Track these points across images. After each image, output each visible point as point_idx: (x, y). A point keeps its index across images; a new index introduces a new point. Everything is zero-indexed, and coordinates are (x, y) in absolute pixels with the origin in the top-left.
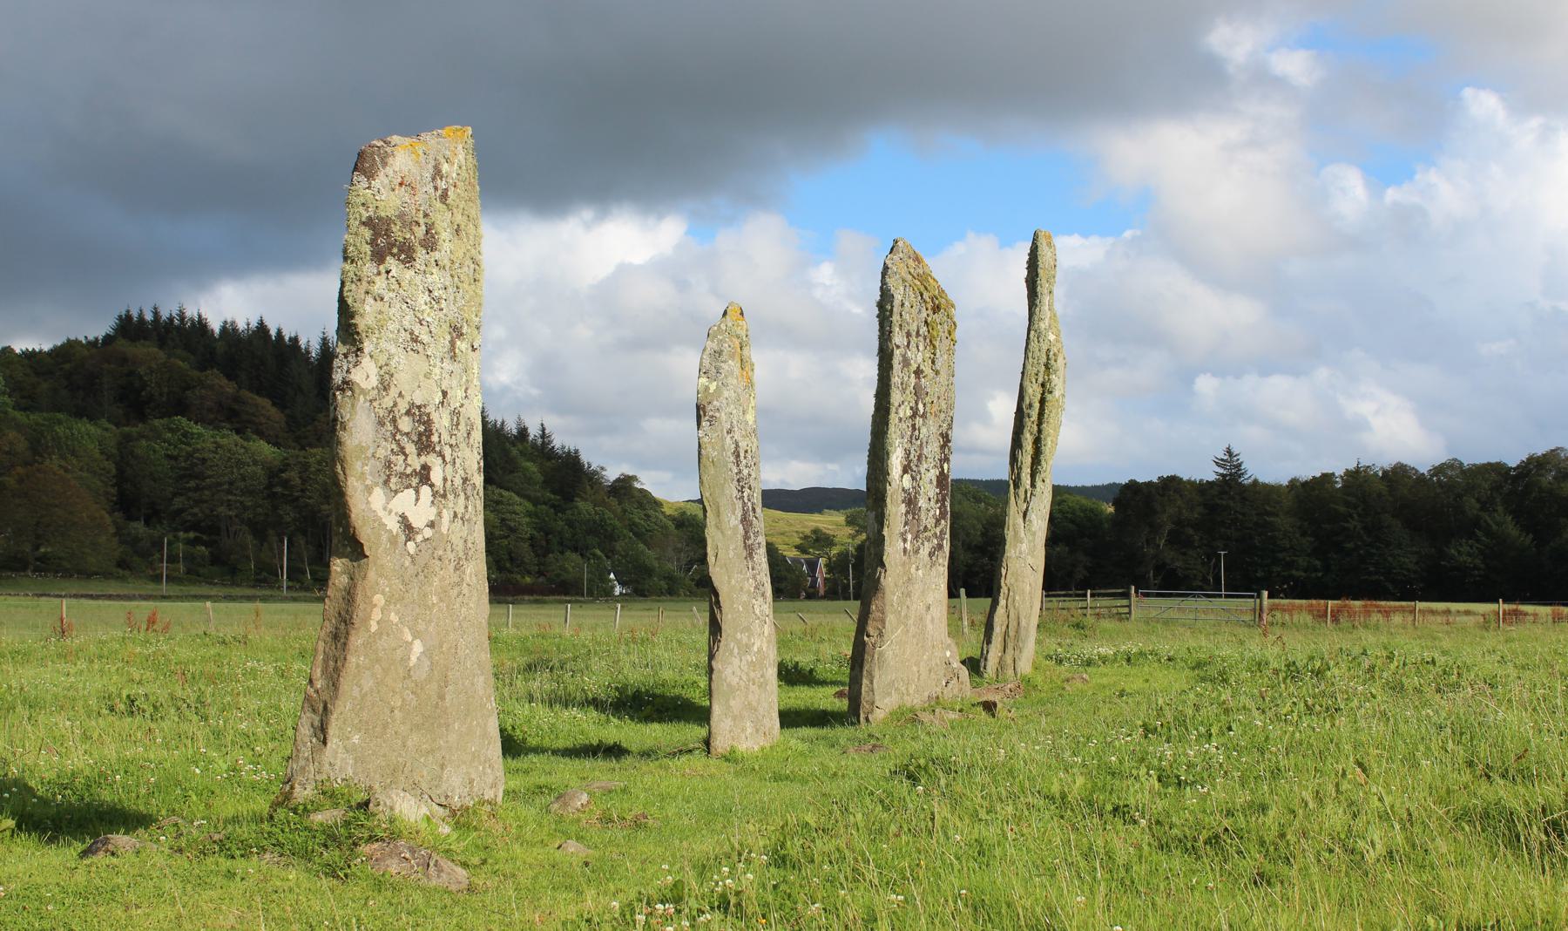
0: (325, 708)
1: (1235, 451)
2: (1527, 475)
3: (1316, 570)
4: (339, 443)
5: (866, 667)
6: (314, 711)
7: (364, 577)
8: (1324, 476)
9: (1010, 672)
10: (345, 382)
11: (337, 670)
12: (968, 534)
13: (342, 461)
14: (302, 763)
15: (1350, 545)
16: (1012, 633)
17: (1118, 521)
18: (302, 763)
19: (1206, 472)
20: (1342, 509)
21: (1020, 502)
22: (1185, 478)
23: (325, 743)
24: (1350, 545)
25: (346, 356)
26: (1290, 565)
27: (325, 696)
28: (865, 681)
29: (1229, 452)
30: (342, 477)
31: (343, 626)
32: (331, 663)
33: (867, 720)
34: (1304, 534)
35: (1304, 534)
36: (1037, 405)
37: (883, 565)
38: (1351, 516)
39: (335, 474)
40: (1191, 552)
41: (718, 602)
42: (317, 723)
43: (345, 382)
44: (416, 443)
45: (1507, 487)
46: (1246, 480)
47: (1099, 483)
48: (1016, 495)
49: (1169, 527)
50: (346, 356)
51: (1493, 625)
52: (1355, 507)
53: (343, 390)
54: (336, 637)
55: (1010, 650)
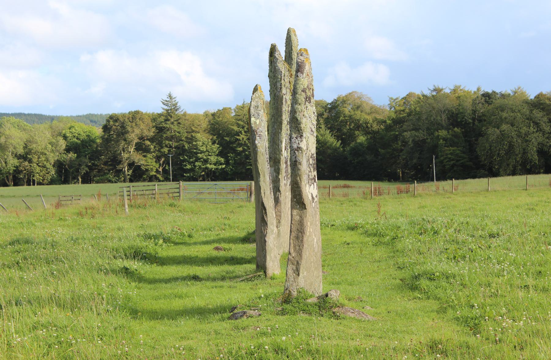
0: (298, 263)
1: (174, 96)
2: (337, 107)
3: (221, 164)
4: (299, 169)
7: (306, 217)
8: (224, 109)
10: (298, 147)
11: (300, 249)
12: (15, 148)
13: (300, 176)
14: (291, 283)
15: (241, 149)
17: (107, 141)
18: (291, 283)
19: (155, 107)
20: (236, 128)
22: (144, 112)
23: (298, 275)
24: (241, 149)
25: (296, 138)
26: (206, 161)
27: (297, 259)
29: (170, 96)
30: (299, 181)
31: (300, 234)
32: (297, 247)
34: (214, 143)
35: (214, 143)
37: (280, 191)
38: (241, 132)
39: (297, 180)
40: (149, 155)
41: (266, 213)
42: (295, 268)
43: (298, 147)
45: (326, 115)
46: (180, 112)
47: (80, 114)
49: (136, 140)
50: (296, 138)
51: (369, 197)
52: (243, 127)
53: (298, 150)
54: (297, 238)
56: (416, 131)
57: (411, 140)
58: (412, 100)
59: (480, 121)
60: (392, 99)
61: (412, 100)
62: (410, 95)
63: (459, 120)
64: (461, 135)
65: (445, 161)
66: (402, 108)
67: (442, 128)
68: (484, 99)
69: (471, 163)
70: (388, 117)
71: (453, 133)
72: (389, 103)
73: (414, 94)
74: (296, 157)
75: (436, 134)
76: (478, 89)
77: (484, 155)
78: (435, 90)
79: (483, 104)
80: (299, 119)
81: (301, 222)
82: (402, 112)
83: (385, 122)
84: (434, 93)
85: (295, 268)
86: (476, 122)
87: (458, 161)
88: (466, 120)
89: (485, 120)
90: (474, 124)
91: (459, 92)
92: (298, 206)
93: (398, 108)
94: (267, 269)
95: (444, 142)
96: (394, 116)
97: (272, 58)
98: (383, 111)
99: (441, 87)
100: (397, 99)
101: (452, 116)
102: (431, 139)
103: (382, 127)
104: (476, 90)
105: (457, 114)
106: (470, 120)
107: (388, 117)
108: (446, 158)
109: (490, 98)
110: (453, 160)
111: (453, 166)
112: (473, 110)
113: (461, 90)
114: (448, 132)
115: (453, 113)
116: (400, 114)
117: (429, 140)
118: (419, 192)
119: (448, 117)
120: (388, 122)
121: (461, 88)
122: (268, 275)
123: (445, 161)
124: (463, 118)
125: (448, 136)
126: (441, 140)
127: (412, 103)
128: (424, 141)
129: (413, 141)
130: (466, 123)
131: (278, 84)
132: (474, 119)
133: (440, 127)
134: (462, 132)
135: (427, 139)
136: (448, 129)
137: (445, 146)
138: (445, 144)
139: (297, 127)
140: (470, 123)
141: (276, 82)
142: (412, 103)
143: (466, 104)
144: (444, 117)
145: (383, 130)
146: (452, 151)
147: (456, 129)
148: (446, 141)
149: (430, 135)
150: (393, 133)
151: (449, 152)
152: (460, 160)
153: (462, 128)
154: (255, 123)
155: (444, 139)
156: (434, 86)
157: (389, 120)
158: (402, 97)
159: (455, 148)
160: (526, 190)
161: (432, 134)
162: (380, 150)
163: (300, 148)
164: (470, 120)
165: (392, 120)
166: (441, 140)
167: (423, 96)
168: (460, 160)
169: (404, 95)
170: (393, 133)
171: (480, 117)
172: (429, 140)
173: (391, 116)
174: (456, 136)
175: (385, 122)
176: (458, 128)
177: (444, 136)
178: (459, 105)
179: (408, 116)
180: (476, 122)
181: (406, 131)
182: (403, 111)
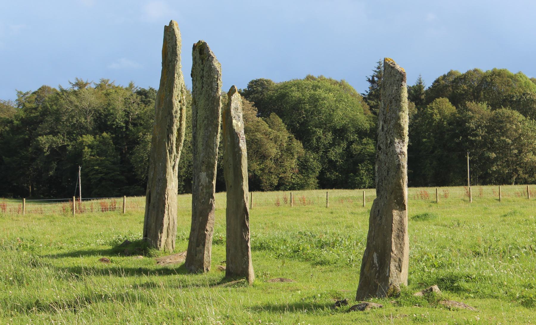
0: (400, 260)
5: (206, 246)
6: (395, 261)
9: (171, 247)
10: (400, 151)
11: (401, 247)
14: (394, 278)
16: (171, 227)
18: (394, 278)
21: (172, 161)
23: (401, 271)
25: (399, 143)
28: (206, 252)
30: (402, 184)
31: (401, 233)
32: (399, 246)
33: (207, 270)
36: (179, 112)
39: (400, 183)
41: (248, 218)
42: (397, 265)
43: (400, 151)
44: (320, 162)
48: (171, 157)
51: (70, 213)
53: (401, 155)
55: (170, 236)
56: (54, 136)
57: (47, 146)
58: (47, 96)
59: (135, 125)
60: (20, 93)
61: (47, 96)
62: (43, 89)
63: (109, 123)
64: (111, 142)
65: (91, 174)
66: (34, 105)
67: (88, 132)
68: (139, 97)
69: (123, 177)
70: (16, 116)
71: (101, 139)
72: (17, 98)
73: (49, 88)
74: (399, 161)
75: (80, 139)
76: (131, 85)
77: (140, 167)
78: (77, 84)
79: (138, 104)
80: (402, 125)
81: (401, 222)
82: (33, 111)
83: (12, 122)
84: (76, 89)
85: (397, 264)
86: (131, 127)
87: (106, 174)
88: (117, 123)
89: (141, 124)
90: (127, 128)
91: (107, 87)
92: (398, 207)
93: (28, 105)
94: (250, 276)
95: (90, 150)
96: (23, 115)
97: (202, 56)
98: (8, 109)
99: (85, 81)
100: (27, 93)
101: (99, 118)
102: (73, 146)
103: (7, 128)
104: (128, 86)
105: (106, 116)
106: (122, 124)
107: (16, 116)
108: (92, 170)
109: (147, 97)
110: (101, 173)
111: (102, 179)
112: (125, 111)
113: (109, 85)
114: (95, 138)
115: (100, 114)
116: (31, 113)
117: (70, 147)
118: (128, 209)
119: (94, 119)
120: (16, 122)
121: (109, 83)
122: (250, 282)
123: (91, 174)
124: (114, 121)
125: (95, 143)
126: (86, 148)
127: (47, 99)
128: (64, 148)
129: (50, 147)
130: (117, 127)
131: (214, 84)
132: (127, 123)
133: (82, 130)
134: (112, 138)
135: (68, 145)
136: (94, 134)
137: (91, 155)
138: (91, 152)
139: (399, 133)
140: (122, 127)
141: (212, 82)
142: (47, 99)
143: (454, 111)
144: (90, 119)
145: (8, 132)
146: (99, 162)
147: (105, 134)
148: (92, 148)
149: (71, 141)
150: (22, 136)
151: (97, 162)
152: (109, 173)
153: (112, 134)
154: (237, 125)
155: (90, 146)
156: (77, 79)
157: (17, 120)
158: (33, 91)
159: (103, 158)
160: (499, 200)
161: (75, 139)
162: (4, 157)
163: (402, 152)
164: (122, 124)
165: (20, 120)
166: (86, 148)
167: (63, 91)
168: (109, 173)
169: (35, 89)
170: (22, 136)
171: (135, 120)
172: (70, 147)
173: (19, 116)
174: (103, 142)
175: (12, 122)
176: (107, 133)
177: (90, 143)
178: (109, 104)
179: (41, 116)
180: (131, 127)
181: (40, 135)
182: (36, 109)
